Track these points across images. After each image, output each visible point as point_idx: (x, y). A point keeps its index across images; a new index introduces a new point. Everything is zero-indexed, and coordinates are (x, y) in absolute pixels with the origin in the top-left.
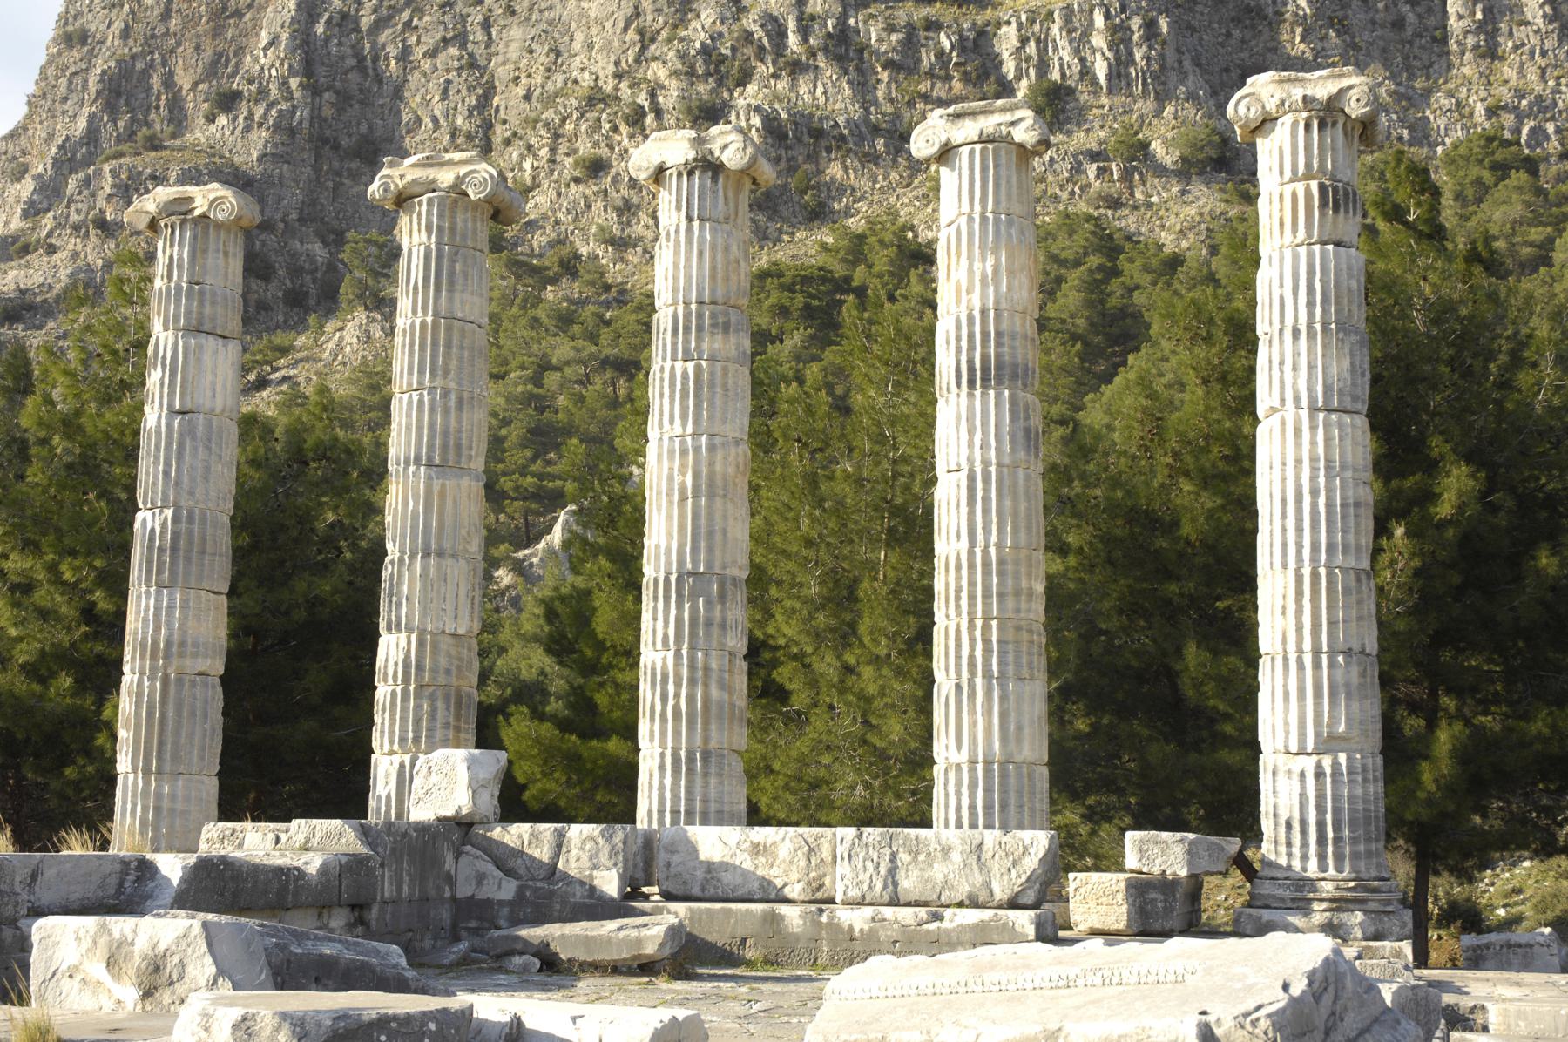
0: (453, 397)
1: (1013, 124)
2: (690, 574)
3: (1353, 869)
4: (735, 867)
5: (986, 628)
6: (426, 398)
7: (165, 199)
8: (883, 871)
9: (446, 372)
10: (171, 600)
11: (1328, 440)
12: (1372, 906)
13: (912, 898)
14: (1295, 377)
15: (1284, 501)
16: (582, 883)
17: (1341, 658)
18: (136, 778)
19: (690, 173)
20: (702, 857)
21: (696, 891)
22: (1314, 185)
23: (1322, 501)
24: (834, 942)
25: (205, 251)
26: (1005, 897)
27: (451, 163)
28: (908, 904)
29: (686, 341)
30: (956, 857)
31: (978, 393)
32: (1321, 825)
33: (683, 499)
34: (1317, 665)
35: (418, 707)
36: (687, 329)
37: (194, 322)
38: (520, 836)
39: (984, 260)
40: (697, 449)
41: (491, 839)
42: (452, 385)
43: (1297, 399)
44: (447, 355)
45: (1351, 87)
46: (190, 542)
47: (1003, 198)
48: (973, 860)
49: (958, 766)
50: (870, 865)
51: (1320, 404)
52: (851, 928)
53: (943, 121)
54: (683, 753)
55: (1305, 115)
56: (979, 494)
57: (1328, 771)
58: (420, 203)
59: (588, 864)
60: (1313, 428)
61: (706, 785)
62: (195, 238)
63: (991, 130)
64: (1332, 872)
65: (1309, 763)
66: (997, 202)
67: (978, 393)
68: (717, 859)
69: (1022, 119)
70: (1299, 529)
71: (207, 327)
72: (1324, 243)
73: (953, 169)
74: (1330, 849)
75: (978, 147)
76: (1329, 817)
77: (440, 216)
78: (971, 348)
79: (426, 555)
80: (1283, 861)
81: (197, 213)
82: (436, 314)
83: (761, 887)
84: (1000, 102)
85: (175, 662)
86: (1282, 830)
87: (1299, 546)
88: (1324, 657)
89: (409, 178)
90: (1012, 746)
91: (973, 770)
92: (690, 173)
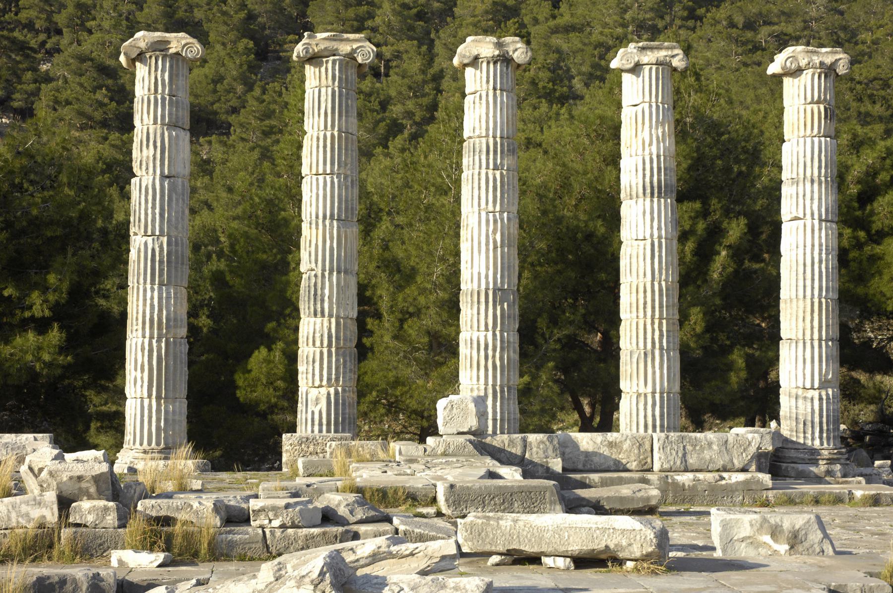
0: (350, 180)
1: (673, 56)
2: (499, 290)
3: (834, 445)
4: (600, 454)
5: (660, 324)
6: (336, 180)
7: (151, 40)
8: (680, 455)
9: (346, 165)
10: (168, 293)
11: (827, 235)
12: (843, 461)
13: (695, 468)
14: (812, 203)
15: (805, 265)
16: (542, 466)
17: (830, 343)
18: (150, 402)
19: (495, 63)
20: (582, 449)
21: (580, 467)
22: (822, 107)
23: (823, 266)
24: (675, 492)
25: (177, 75)
26: (741, 466)
27: (348, 40)
28: (692, 471)
29: (495, 159)
30: (715, 447)
31: (655, 200)
32: (821, 423)
33: (495, 248)
34: (820, 346)
35: (337, 360)
36: (495, 152)
37: (174, 120)
38: (503, 442)
39: (657, 128)
40: (502, 220)
41: (485, 443)
42: (349, 173)
43: (812, 214)
44: (346, 154)
45: (840, 59)
46: (177, 258)
47: (666, 95)
48: (723, 449)
49: (645, 395)
50: (674, 453)
51: (824, 217)
52: (684, 484)
53: (635, 51)
54: (498, 388)
55: (819, 70)
56: (657, 254)
57: (824, 397)
58: (327, 62)
59: (543, 456)
60: (820, 229)
61: (508, 405)
62: (171, 67)
63: (662, 59)
64: (825, 445)
65: (816, 394)
66: (663, 98)
67: (655, 200)
68: (591, 449)
69: (677, 55)
70: (813, 280)
71: (180, 124)
73: (638, 76)
74: (825, 435)
75: (654, 67)
76: (824, 420)
77: (340, 71)
78: (652, 175)
79: (339, 272)
80: (801, 441)
81: (172, 51)
82: (340, 130)
83: (615, 464)
84: (666, 44)
85: (172, 331)
86: (801, 426)
87: (813, 288)
88: (823, 343)
89: (322, 47)
90: (672, 384)
91: (654, 397)
92: (495, 63)
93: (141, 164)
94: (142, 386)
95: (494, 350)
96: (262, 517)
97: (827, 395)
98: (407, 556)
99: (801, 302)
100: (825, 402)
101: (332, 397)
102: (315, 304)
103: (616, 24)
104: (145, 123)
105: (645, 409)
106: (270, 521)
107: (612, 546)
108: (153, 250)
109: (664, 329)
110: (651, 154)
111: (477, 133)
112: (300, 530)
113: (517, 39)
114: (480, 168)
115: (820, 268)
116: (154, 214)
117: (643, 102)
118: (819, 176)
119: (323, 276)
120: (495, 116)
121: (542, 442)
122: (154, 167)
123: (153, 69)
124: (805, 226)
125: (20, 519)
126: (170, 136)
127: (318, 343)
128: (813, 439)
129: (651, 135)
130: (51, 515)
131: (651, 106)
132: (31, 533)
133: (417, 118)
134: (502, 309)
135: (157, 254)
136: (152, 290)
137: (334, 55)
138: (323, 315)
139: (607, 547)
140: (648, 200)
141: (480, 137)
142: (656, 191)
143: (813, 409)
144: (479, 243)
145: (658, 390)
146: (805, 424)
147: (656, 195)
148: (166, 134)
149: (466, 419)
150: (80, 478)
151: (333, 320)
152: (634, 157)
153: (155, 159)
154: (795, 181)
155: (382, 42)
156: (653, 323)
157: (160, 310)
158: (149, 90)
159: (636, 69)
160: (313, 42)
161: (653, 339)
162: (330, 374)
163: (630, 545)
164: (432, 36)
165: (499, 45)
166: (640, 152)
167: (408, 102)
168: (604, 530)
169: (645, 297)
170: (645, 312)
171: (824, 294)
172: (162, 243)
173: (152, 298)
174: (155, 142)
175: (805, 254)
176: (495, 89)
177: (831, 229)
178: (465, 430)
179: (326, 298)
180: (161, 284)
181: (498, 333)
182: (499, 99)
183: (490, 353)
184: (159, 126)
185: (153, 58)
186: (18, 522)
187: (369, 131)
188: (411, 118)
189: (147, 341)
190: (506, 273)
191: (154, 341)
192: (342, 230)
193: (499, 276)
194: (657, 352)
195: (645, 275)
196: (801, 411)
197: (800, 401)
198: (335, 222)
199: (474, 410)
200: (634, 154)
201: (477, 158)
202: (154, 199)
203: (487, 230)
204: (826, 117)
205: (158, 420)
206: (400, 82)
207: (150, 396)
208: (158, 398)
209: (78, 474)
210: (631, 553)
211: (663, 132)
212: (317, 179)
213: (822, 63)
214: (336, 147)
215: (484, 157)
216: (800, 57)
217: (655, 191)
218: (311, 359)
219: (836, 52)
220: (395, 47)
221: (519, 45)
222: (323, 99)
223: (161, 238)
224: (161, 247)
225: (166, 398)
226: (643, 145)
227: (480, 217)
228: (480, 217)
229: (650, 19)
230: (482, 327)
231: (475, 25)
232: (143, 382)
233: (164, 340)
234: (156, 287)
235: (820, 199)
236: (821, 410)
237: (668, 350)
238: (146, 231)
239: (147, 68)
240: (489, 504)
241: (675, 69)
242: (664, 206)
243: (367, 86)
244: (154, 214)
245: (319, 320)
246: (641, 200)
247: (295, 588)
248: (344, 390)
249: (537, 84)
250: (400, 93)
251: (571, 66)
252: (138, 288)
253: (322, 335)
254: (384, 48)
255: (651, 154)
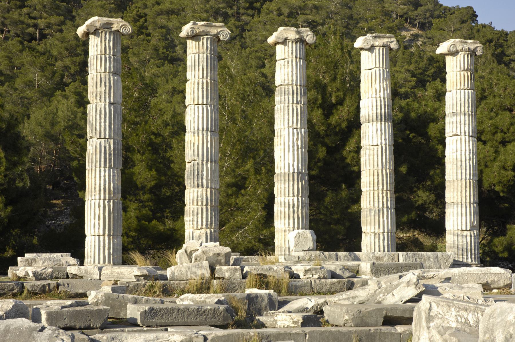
1: (391, 42)
2: (300, 173)
6: (209, 108)
7: (103, 22)
9: (214, 99)
10: (114, 173)
14: (465, 127)
17: (475, 205)
18: (104, 238)
19: (296, 42)
23: (471, 162)
25: (117, 43)
27: (215, 26)
29: (297, 98)
30: (432, 260)
31: (383, 123)
32: (471, 249)
33: (298, 149)
35: (211, 213)
37: (116, 70)
39: (383, 83)
40: (301, 133)
43: (465, 133)
53: (371, 38)
56: (384, 154)
57: (473, 235)
58: (203, 39)
60: (469, 141)
62: (114, 38)
63: (386, 43)
64: (474, 262)
65: (468, 233)
66: (386, 65)
67: (383, 123)
69: (393, 41)
70: (466, 169)
72: (471, 90)
73: (372, 53)
74: (473, 256)
75: (381, 48)
76: (473, 248)
78: (381, 109)
79: (211, 162)
80: (461, 260)
81: (113, 29)
82: (211, 79)
87: (466, 174)
88: (472, 205)
91: (384, 235)
92: (296, 42)
93: (96, 96)
94: (99, 228)
95: (298, 208)
96: (309, 274)
97: (474, 234)
98: (431, 278)
99: (459, 182)
100: (473, 238)
101: (209, 235)
102: (198, 180)
103: (202, 11)
104: (98, 71)
105: (379, 242)
106: (313, 275)
107: (489, 282)
108: (105, 147)
109: (389, 196)
110: (380, 97)
111: (286, 82)
112: (327, 280)
113: (308, 29)
114: (289, 103)
115: (469, 163)
116: (105, 126)
117: (376, 67)
118: (468, 111)
119: (203, 164)
120: (296, 73)
121: (346, 256)
122: (105, 97)
123: (103, 39)
124: (461, 139)
125: (192, 275)
126: (114, 79)
127: (200, 203)
128: (467, 259)
129: (380, 86)
130: (207, 274)
131: (380, 70)
132: (200, 282)
133: (72, 71)
134: (302, 184)
135: (107, 150)
136: (105, 171)
137: (207, 35)
138: (203, 187)
139: (487, 282)
140: (379, 123)
141: (288, 85)
142: (383, 118)
143: (467, 242)
144: (289, 146)
145: (386, 231)
146: (462, 250)
147: (383, 120)
148: (112, 78)
149: (307, 243)
150: (219, 254)
151: (209, 190)
152: (370, 99)
153: (105, 93)
154: (454, 114)
155: (38, 16)
156: (383, 193)
157: (110, 183)
158: (101, 52)
159: (371, 49)
160: (196, 27)
161: (383, 202)
162: (207, 221)
163: (499, 280)
164: (74, 14)
165: (298, 32)
166: (374, 96)
167: (65, 60)
168: (485, 274)
169: (378, 178)
170: (378, 187)
171: (472, 177)
172: (110, 143)
173: (105, 176)
174: (105, 83)
175: (461, 155)
176: (296, 58)
177: (475, 141)
178: (307, 249)
179: (204, 177)
180: (110, 168)
181: (300, 198)
182: (298, 64)
183: (296, 209)
184: (107, 74)
185: (104, 33)
186: (191, 277)
187: (47, 79)
188: (67, 71)
189: (102, 201)
190: (304, 164)
191: (106, 201)
192: (213, 137)
193: (300, 165)
194: (385, 210)
195: (378, 165)
196: (460, 243)
197: (460, 238)
198: (209, 133)
199: (311, 238)
200: (370, 96)
201: (286, 97)
202: (105, 117)
203: (293, 139)
204: (471, 79)
205: (109, 249)
206: (60, 45)
207: (104, 234)
208: (109, 235)
209: (218, 252)
210: (498, 285)
211: (386, 85)
212: (198, 107)
213: (469, 49)
214: (209, 88)
215: (291, 97)
216: (458, 45)
217: (382, 118)
218: (196, 213)
219: (476, 43)
220: (48, 20)
221: (309, 33)
222: (201, 60)
223: (109, 140)
224: (110, 145)
225: (113, 236)
226: (373, 93)
227: (289, 131)
228: (289, 131)
229: (223, 8)
230: (291, 195)
231: (102, 7)
232: (99, 226)
233: (112, 201)
234: (107, 169)
235: (469, 124)
236: (471, 242)
237: (391, 208)
238: (100, 136)
239: (100, 38)
240: (391, 272)
241: (391, 49)
242: (387, 127)
243: (42, 48)
244: (105, 126)
245: (200, 190)
246: (375, 123)
247: (406, 287)
248: (214, 231)
249: (158, 51)
250: (60, 53)
251: (175, 38)
252: (95, 170)
253: (202, 199)
254: (39, 21)
255: (380, 97)
